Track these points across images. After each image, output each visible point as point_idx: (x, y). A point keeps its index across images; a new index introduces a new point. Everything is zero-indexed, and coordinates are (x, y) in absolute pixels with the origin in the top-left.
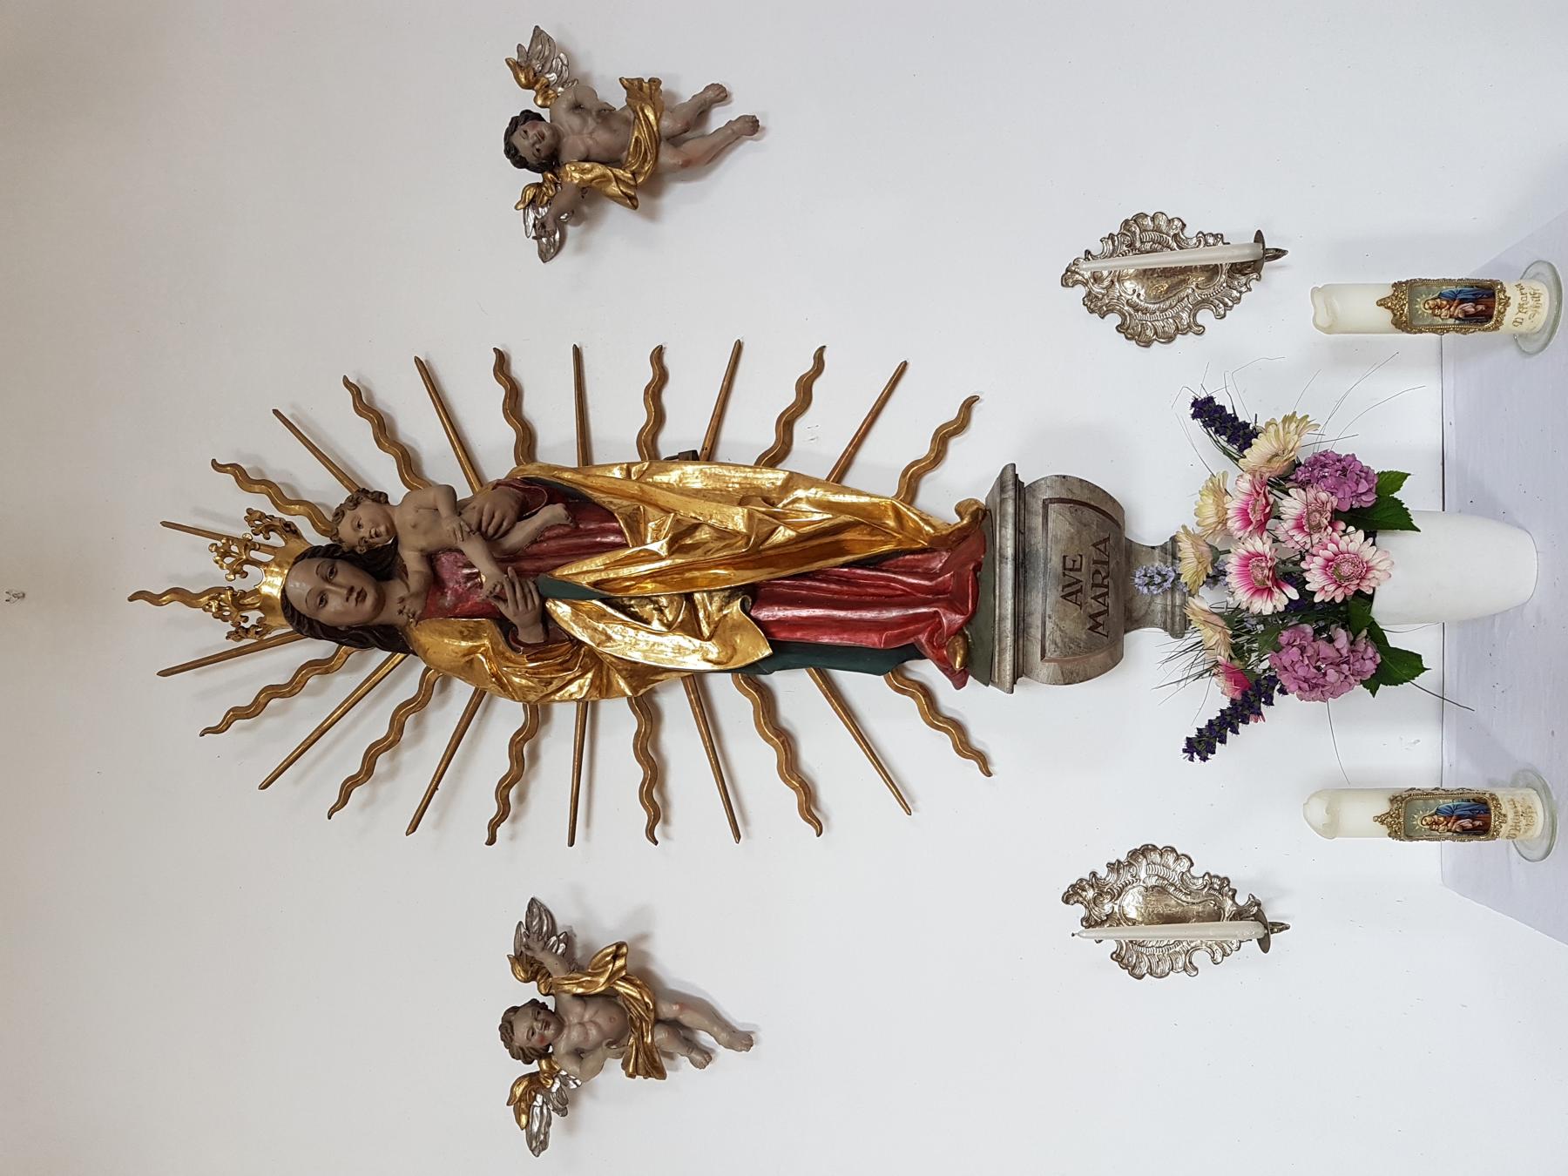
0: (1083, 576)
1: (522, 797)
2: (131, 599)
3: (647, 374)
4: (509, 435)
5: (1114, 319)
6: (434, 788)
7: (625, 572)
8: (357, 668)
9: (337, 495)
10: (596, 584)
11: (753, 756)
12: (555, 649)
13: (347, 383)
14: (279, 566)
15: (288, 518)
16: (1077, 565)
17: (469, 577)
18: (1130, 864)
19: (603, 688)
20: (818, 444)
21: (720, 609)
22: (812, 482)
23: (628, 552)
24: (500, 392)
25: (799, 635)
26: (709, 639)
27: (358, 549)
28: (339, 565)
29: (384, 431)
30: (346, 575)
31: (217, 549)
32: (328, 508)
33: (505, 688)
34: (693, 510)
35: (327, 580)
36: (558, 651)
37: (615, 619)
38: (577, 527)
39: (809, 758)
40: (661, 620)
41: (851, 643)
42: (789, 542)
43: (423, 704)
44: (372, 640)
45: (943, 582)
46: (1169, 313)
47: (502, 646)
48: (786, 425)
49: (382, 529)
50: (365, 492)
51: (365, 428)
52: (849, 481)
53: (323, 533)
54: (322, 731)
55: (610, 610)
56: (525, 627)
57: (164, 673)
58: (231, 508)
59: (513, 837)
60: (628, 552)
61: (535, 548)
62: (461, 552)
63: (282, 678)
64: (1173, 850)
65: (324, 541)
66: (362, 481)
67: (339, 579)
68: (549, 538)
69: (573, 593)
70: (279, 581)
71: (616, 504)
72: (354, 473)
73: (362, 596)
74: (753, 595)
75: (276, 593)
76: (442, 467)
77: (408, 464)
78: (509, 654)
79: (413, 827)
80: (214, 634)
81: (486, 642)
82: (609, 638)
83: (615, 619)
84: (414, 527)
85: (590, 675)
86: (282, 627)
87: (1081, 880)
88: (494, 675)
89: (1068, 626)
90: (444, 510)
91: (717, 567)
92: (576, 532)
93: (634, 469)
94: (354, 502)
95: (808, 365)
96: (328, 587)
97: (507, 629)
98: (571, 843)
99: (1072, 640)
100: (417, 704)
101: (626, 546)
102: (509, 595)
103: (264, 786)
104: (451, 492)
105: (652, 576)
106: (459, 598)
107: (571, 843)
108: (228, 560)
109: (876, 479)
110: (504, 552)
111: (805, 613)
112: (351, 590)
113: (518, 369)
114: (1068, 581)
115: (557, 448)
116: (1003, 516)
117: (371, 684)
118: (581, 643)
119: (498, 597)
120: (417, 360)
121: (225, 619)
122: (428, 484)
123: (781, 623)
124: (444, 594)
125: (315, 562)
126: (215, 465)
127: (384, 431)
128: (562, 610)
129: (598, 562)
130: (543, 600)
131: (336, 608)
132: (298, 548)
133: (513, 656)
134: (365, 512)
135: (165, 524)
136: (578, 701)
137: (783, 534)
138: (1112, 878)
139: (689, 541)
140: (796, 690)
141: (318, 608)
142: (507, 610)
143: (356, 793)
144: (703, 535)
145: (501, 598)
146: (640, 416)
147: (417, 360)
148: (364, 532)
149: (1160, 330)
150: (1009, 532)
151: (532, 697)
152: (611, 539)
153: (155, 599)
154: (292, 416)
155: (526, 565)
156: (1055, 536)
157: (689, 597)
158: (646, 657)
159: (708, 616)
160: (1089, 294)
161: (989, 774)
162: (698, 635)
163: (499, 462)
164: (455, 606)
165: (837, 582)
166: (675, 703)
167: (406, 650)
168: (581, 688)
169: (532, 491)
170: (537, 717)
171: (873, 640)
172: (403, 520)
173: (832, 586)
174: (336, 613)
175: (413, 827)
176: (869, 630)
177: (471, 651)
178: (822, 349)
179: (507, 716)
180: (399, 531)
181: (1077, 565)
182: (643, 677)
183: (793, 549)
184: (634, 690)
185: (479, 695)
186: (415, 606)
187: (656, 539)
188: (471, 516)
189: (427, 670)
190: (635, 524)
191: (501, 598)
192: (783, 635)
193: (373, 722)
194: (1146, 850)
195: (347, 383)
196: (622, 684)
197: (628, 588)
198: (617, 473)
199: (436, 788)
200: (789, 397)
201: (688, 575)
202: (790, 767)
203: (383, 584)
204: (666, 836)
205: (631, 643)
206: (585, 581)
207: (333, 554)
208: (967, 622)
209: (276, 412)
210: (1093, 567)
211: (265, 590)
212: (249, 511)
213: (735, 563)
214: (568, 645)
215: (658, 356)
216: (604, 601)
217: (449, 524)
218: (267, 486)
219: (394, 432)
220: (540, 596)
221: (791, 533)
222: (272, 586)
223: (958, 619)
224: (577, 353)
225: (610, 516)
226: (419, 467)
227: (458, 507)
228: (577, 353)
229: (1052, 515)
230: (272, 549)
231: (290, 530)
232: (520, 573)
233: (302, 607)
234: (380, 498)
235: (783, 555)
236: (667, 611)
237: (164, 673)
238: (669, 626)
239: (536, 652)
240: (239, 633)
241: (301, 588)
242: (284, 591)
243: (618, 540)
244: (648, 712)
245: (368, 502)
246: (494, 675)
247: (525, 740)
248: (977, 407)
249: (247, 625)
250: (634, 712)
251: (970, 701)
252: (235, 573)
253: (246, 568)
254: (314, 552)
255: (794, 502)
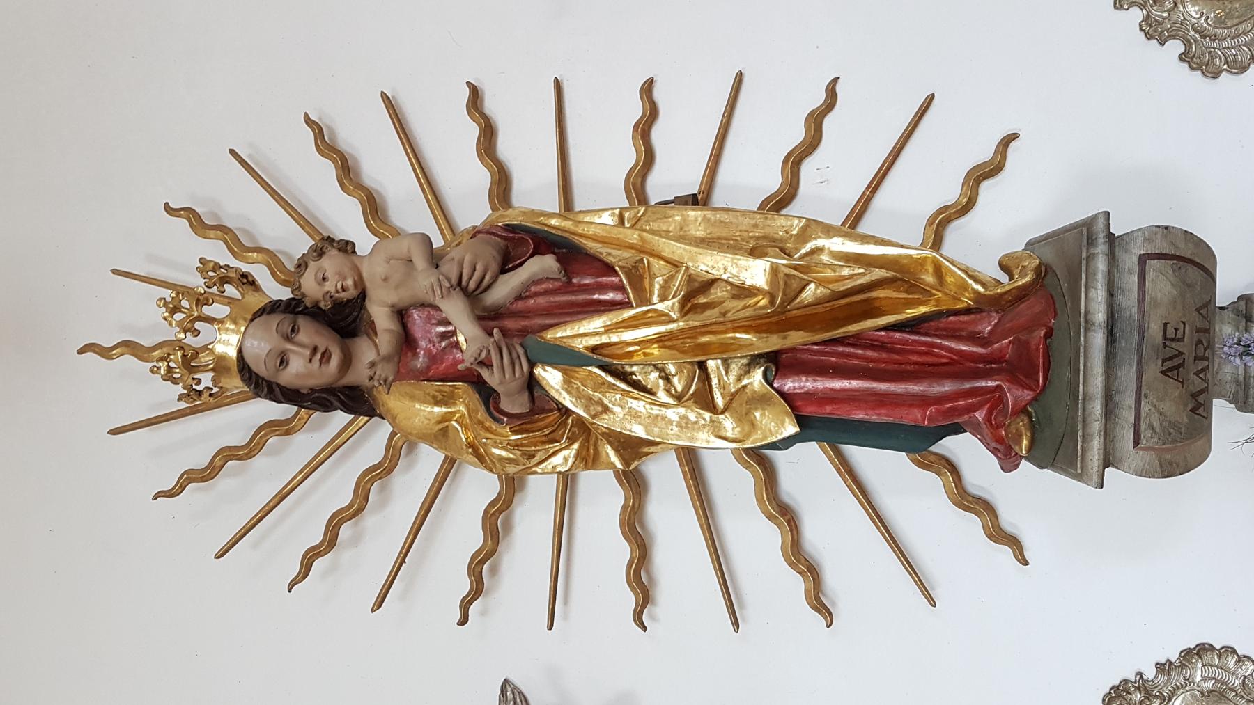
0: (1186, 347)
1: (494, 571)
2: (81, 352)
3: (636, 110)
4: (482, 177)
5: (1176, 47)
6: (401, 560)
7: (629, 336)
8: (319, 427)
9: (301, 244)
10: (594, 349)
11: (752, 537)
12: (543, 419)
13: (308, 121)
14: (235, 322)
15: (245, 268)
16: (1179, 335)
17: (444, 336)
18: (1182, 666)
19: (589, 459)
20: (829, 186)
21: (739, 379)
22: (829, 231)
23: (632, 312)
24: (473, 131)
25: (828, 409)
26: (723, 412)
27: (322, 305)
28: (302, 322)
29: (347, 172)
30: (308, 333)
31: (166, 304)
32: (289, 257)
33: (482, 459)
34: (710, 263)
35: (288, 339)
36: (540, 418)
37: (613, 387)
38: (569, 282)
39: (814, 536)
40: (668, 391)
41: (890, 420)
42: (818, 302)
43: (389, 471)
44: (336, 403)
45: (1000, 350)
46: (1243, 39)
47: (481, 414)
48: (794, 162)
49: (350, 282)
50: (330, 240)
51: (327, 169)
52: (864, 227)
53: (284, 283)
54: (281, 497)
55: (610, 379)
56: (509, 395)
57: (114, 432)
58: (185, 254)
59: (484, 613)
60: (632, 312)
61: (520, 305)
62: (439, 310)
63: (239, 438)
64: (1234, 651)
65: (284, 294)
66: (326, 229)
67: (302, 337)
68: (537, 294)
69: (566, 358)
70: (234, 339)
71: (614, 256)
72: (315, 218)
73: (326, 356)
74: (777, 363)
75: (233, 353)
76: (411, 215)
77: (374, 208)
78: (489, 423)
79: (379, 603)
80: (169, 395)
81: (462, 408)
82: (606, 410)
83: (613, 387)
84: (385, 280)
85: (576, 446)
86: (235, 384)
87: (1126, 681)
88: (471, 445)
89: (1168, 407)
90: (420, 262)
91: (735, 330)
92: (568, 287)
93: (627, 215)
94: (318, 252)
95: (819, 99)
96: (289, 346)
97: (488, 396)
98: (550, 627)
99: (1172, 424)
100: (382, 471)
101: (627, 305)
102: (494, 362)
103: (220, 555)
104: (427, 240)
105: (661, 340)
106: (433, 359)
107: (550, 627)
108: (179, 316)
109: (898, 226)
110: (485, 309)
111: (838, 384)
112: (315, 350)
113: (491, 106)
114: (1169, 352)
115: (535, 194)
116: (1091, 276)
117: (332, 448)
118: (568, 412)
119: (482, 363)
120: (384, 96)
121: (175, 382)
122: (397, 233)
123: (809, 396)
124: (416, 355)
125: (275, 319)
126: (167, 207)
127: (347, 172)
128: (551, 377)
129: (596, 323)
130: (532, 365)
131: (299, 370)
132: (256, 302)
133: (494, 426)
134: (331, 262)
135: (115, 272)
136: (559, 473)
137: (811, 292)
138: (1162, 679)
139: (702, 300)
140: (806, 469)
141: (278, 370)
142: (492, 378)
143: (318, 564)
144: (717, 293)
145: (486, 364)
146: (628, 157)
147: (384, 96)
148: (329, 286)
149: (1231, 58)
150: (1099, 294)
151: (511, 469)
152: (610, 296)
153: (105, 353)
154: (250, 156)
155: (510, 324)
156: (1154, 300)
157: (702, 365)
158: (648, 433)
159: (723, 387)
160: (1147, 19)
161: (1025, 563)
162: (711, 407)
163: (473, 210)
164: (428, 368)
165: (872, 347)
166: (664, 474)
167: (371, 412)
168: (566, 460)
169: (516, 241)
170: (512, 487)
171: (915, 416)
172: (373, 272)
173: (870, 353)
174: (297, 375)
175: (379, 603)
176: (911, 406)
177: (445, 419)
178: (836, 80)
179: (477, 487)
180: (368, 285)
181: (1179, 335)
182: (632, 448)
183: (820, 309)
184: (626, 463)
185: (449, 467)
186: (385, 371)
187: (663, 298)
188: (450, 269)
189: (393, 434)
190: (638, 276)
191: (486, 364)
192: (809, 410)
193: (335, 487)
194: (1202, 649)
195: (308, 121)
196: (612, 453)
197: (630, 354)
198: (607, 219)
199: (403, 561)
200: (797, 135)
201: (704, 339)
202: (798, 555)
203: (347, 340)
204: (653, 618)
205: (626, 414)
206: (580, 345)
207: (294, 308)
208: (1035, 399)
209: (232, 152)
210: (1196, 337)
211: (219, 349)
212: (202, 260)
213: (759, 325)
214: (556, 414)
215: (647, 89)
216: (602, 368)
217: (424, 282)
218: (223, 232)
219: (358, 174)
220: (529, 360)
221: (821, 291)
222: (227, 344)
223: (1027, 395)
224: (558, 86)
225: (609, 269)
226: (385, 211)
227: (435, 259)
228: (558, 86)
229: (1150, 275)
230: (230, 301)
231: (246, 281)
232: (504, 332)
233: (260, 369)
234: (347, 248)
235: (807, 320)
236: (675, 380)
237: (114, 432)
238: (679, 398)
239: (520, 422)
240: (192, 394)
241: (261, 347)
242: (240, 351)
243: (619, 297)
244: (635, 484)
245: (334, 252)
246: (471, 445)
247: (500, 511)
248: (1013, 145)
249: (199, 388)
250: (621, 484)
251: (1028, 492)
252: (185, 331)
253: (198, 325)
254: (274, 307)
255: (813, 252)
